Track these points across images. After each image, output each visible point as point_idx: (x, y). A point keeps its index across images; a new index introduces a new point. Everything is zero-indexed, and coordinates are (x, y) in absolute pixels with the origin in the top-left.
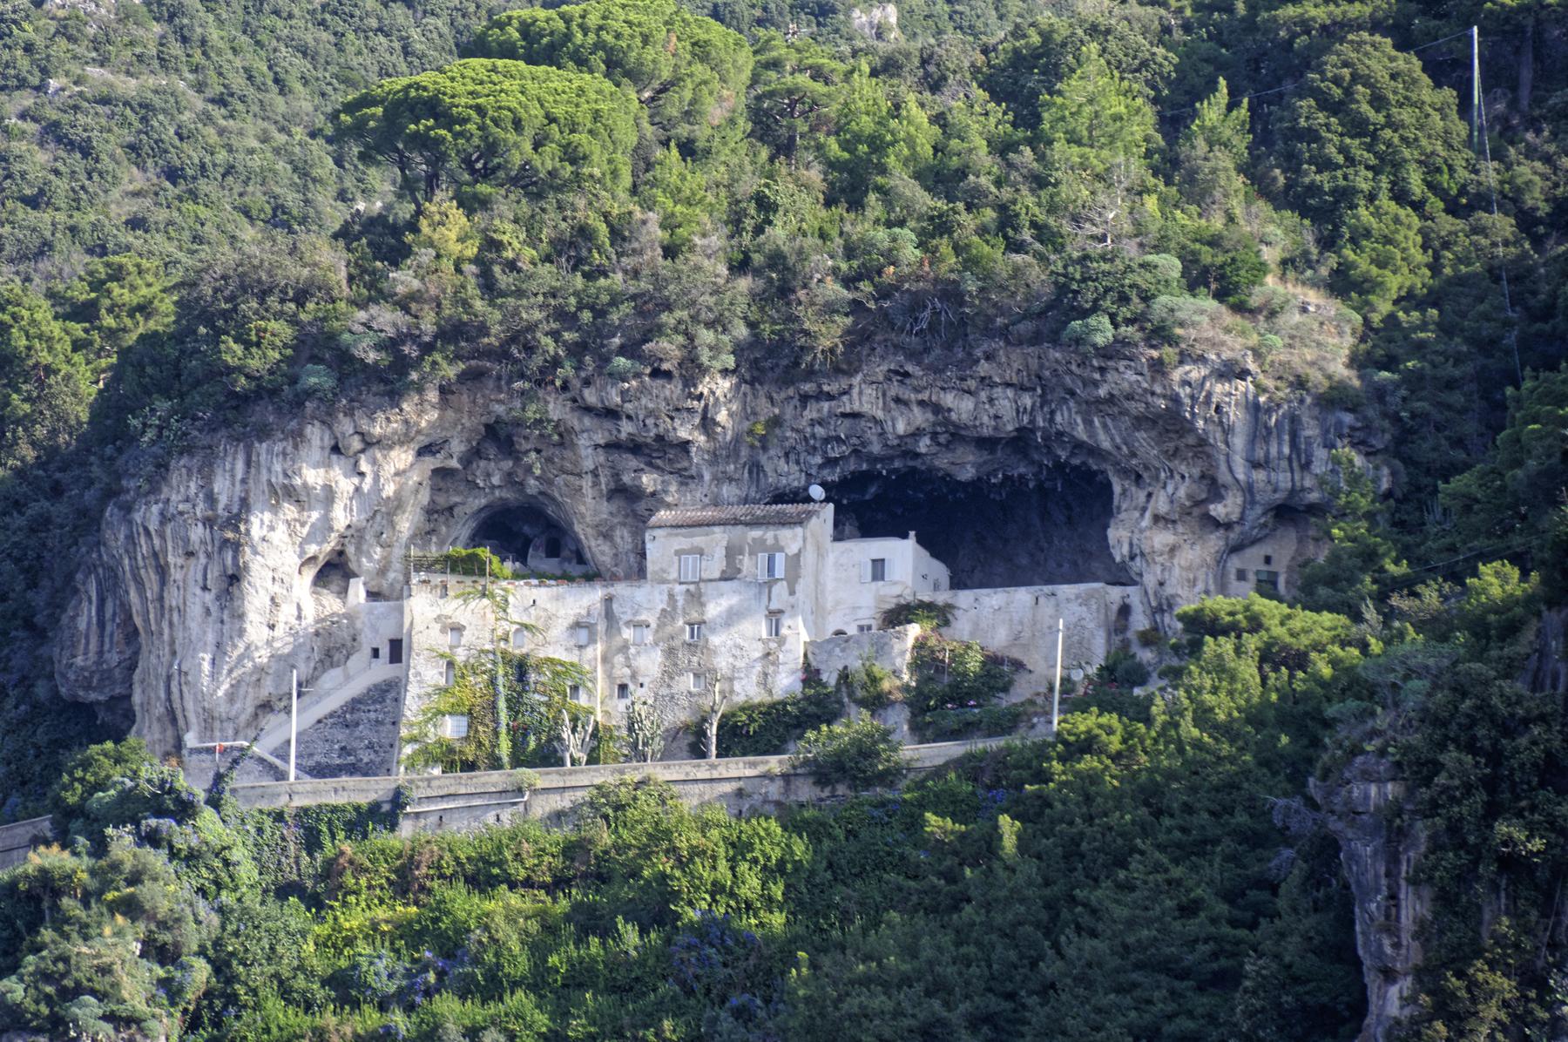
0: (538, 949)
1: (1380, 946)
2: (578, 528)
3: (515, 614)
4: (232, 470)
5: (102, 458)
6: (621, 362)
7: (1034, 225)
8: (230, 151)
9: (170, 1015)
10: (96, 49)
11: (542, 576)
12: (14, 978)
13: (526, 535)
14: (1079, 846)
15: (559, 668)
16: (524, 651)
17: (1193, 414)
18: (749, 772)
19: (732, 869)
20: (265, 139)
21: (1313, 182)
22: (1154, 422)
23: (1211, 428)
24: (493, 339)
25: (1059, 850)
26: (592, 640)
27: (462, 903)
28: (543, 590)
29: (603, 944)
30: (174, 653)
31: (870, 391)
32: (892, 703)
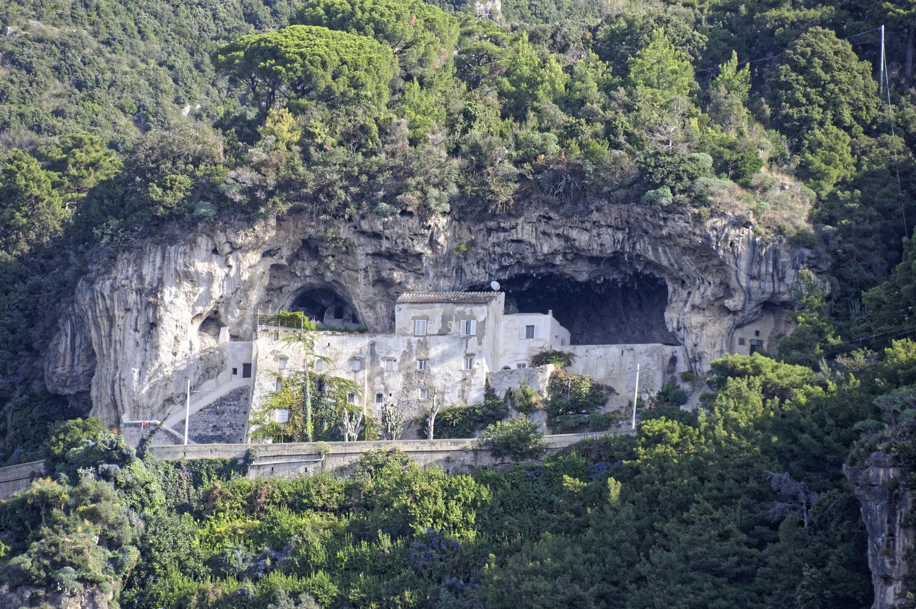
0: (331, 548)
1: (883, 563)
2: (355, 302)
3: (317, 351)
4: (154, 261)
5: (76, 252)
6: (384, 206)
7: (626, 133)
8: (113, 72)
9: (116, 579)
10: (35, 10)
11: (333, 329)
12: (25, 555)
13: (324, 305)
14: (660, 497)
15: (342, 383)
16: (323, 373)
17: (717, 247)
18: (454, 448)
19: (446, 504)
20: (133, 66)
21: (788, 113)
22: (694, 251)
23: (727, 255)
24: (309, 190)
25: (645, 499)
26: (362, 368)
27: (286, 519)
28: (334, 338)
29: (370, 546)
30: (117, 368)
31: (528, 227)
32: (538, 410)
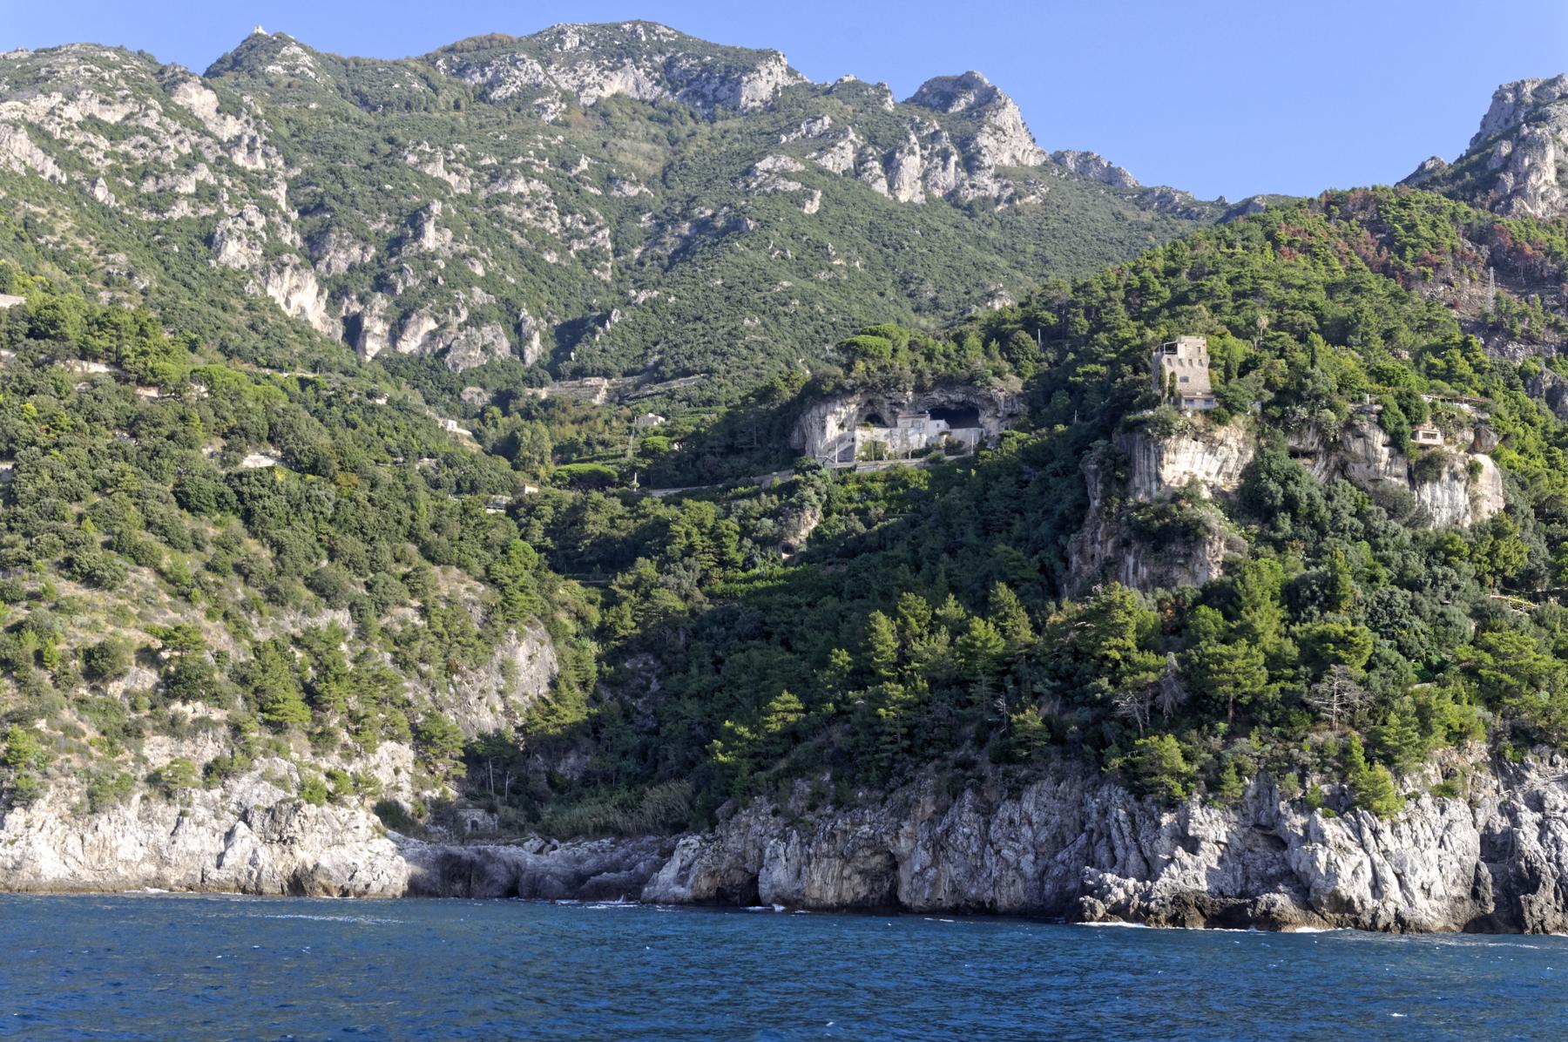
13: (874, 419)
14: (991, 475)
27: (870, 485)
